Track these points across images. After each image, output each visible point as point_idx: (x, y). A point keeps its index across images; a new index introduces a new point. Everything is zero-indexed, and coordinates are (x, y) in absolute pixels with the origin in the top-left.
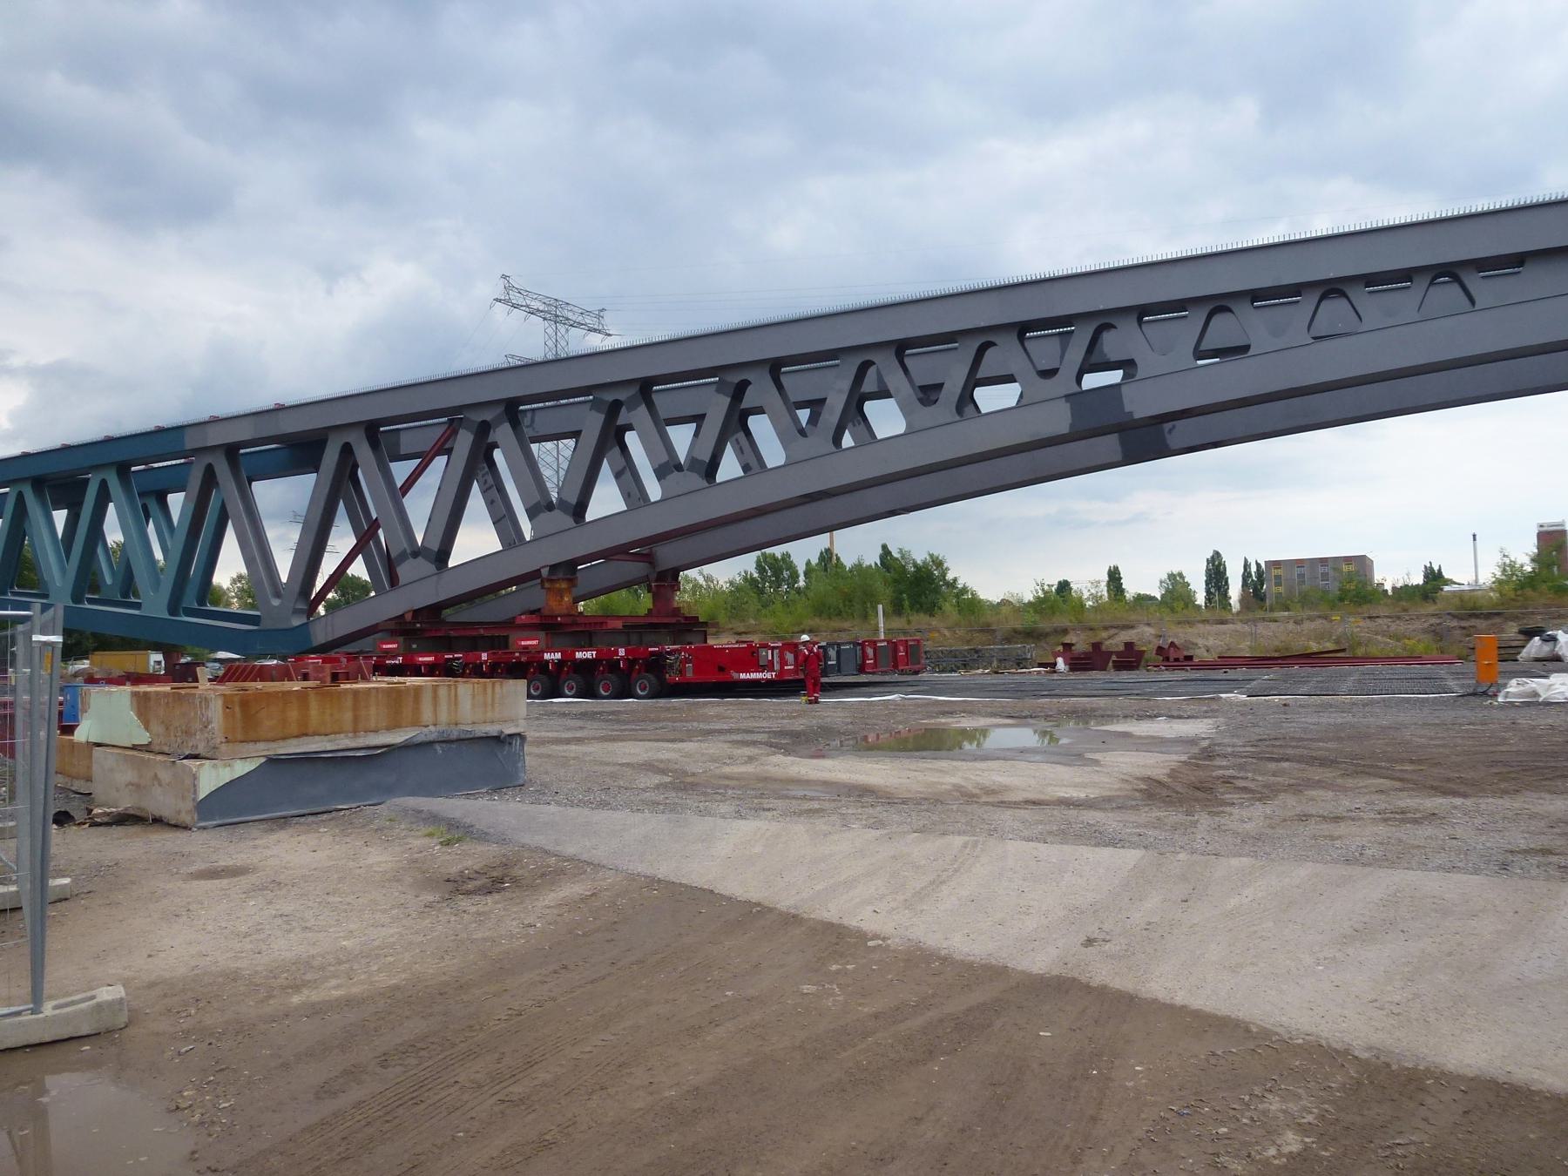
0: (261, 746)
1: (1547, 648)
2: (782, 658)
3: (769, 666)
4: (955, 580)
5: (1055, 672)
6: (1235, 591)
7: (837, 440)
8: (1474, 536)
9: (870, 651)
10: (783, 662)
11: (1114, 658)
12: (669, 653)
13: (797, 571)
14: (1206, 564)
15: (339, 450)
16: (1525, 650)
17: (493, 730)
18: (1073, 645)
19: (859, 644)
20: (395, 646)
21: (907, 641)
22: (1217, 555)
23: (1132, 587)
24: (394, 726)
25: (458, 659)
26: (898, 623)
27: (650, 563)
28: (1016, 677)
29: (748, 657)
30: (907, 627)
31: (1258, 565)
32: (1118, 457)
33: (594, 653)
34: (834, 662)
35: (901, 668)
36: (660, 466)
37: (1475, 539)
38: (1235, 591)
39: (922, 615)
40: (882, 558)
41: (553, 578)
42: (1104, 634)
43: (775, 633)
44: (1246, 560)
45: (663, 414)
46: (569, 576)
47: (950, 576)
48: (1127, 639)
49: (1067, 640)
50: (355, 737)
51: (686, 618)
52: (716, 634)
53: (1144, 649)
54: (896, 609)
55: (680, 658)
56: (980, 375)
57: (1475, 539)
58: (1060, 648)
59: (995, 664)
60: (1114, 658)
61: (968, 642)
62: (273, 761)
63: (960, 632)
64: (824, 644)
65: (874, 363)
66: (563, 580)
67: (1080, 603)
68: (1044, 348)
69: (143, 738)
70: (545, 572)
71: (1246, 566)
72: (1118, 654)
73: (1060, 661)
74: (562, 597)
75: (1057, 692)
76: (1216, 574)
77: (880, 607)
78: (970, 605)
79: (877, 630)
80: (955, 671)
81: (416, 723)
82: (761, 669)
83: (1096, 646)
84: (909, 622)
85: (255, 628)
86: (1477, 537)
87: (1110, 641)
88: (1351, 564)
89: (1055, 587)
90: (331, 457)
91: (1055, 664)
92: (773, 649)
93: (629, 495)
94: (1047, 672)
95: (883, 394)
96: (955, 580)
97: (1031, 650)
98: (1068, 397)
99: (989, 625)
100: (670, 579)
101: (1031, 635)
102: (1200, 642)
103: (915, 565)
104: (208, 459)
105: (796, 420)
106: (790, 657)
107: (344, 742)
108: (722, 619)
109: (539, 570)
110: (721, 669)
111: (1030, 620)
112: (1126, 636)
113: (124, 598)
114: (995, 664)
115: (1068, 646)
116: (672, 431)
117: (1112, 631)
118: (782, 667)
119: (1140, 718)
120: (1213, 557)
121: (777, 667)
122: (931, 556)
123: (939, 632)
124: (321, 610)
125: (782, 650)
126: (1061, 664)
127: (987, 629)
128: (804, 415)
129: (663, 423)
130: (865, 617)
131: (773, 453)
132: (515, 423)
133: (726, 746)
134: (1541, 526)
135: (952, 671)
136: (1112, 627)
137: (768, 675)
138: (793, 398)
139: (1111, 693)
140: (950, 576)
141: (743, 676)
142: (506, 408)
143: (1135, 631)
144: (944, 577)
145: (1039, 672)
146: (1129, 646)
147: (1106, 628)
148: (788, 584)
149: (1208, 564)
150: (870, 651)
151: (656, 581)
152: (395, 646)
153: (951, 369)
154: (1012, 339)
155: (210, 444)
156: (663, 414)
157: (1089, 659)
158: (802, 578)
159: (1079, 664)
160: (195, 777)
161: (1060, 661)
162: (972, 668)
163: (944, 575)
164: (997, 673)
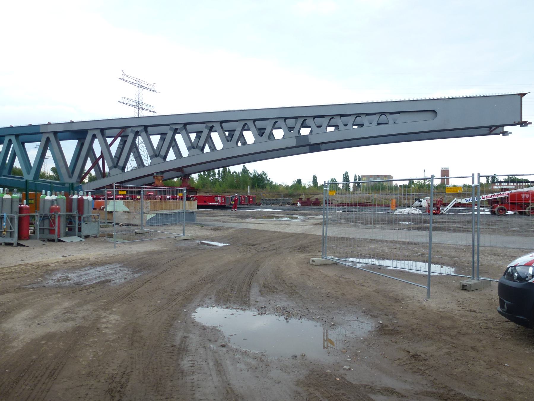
0: (156, 211)
1: (419, 203)
2: (221, 199)
3: (218, 201)
4: (269, 179)
5: (297, 206)
6: (351, 186)
7: (237, 143)
8: (424, 170)
9: (243, 199)
10: (222, 200)
11: (313, 202)
12: (191, 197)
13: (215, 173)
14: (343, 175)
15: (92, 136)
16: (414, 204)
17: (191, 210)
18: (302, 199)
19: (240, 197)
20: (110, 193)
21: (252, 196)
22: (347, 173)
23: (320, 183)
24: (176, 209)
25: (130, 197)
26: (254, 191)
27: (182, 172)
28: (287, 207)
29: (213, 199)
30: (256, 192)
31: (359, 177)
32: (309, 151)
33: (170, 197)
34: (223, 202)
35: (250, 203)
36: (189, 147)
37: (424, 171)
38: (351, 186)
39: (260, 189)
40: (243, 169)
41: (157, 176)
42: (311, 196)
43: (217, 193)
44: (355, 175)
45: (107, 135)
46: (162, 176)
47: (268, 178)
48: (317, 198)
49: (301, 197)
50: (170, 210)
51: (191, 188)
52: (199, 192)
53: (321, 200)
54: (253, 187)
55: (194, 198)
56: (275, 127)
57: (424, 171)
58: (299, 199)
59: (281, 203)
60: (313, 202)
61: (273, 197)
62: (158, 214)
63: (271, 194)
64: (231, 196)
65: (247, 124)
66: (160, 176)
67: (305, 187)
68: (291, 122)
69: (128, 210)
70: (155, 174)
71: (355, 177)
72: (314, 202)
73: (299, 203)
74: (159, 181)
75: (298, 210)
76: (346, 178)
77: (249, 186)
78: (274, 188)
79: (247, 192)
80: (270, 205)
81: (179, 209)
82: (216, 202)
83: (308, 199)
84: (257, 191)
85: (63, 186)
86: (425, 171)
87: (312, 198)
88: (372, 178)
89: (297, 181)
90: (44, 139)
91: (297, 204)
92: (219, 197)
93: (176, 153)
94: (295, 206)
95: (249, 130)
96: (269, 179)
97: (290, 200)
98: (295, 137)
99: (279, 192)
100: (187, 177)
101: (291, 195)
102: (336, 199)
103: (258, 174)
104: (47, 135)
105: (225, 134)
106: (223, 199)
107: (168, 211)
108: (200, 188)
109: (153, 174)
110: (205, 202)
111: (289, 191)
112: (316, 197)
113: (9, 175)
114: (281, 203)
115: (301, 199)
116: (191, 135)
117: (313, 195)
118: (221, 202)
119: (317, 215)
120: (345, 174)
121: (220, 201)
122: (263, 172)
123: (265, 194)
124: (86, 180)
125: (221, 197)
126: (299, 203)
127: (279, 194)
128: (227, 133)
129: (188, 133)
130: (244, 189)
131: (219, 145)
132: (146, 132)
133: (228, 218)
134: (442, 168)
135: (269, 205)
136: (313, 194)
137: (218, 204)
138: (225, 129)
139: (311, 210)
140: (268, 178)
141: (211, 204)
142: (144, 127)
143: (319, 196)
144: (266, 178)
145: (293, 206)
146: (317, 199)
147: (311, 195)
148: (212, 177)
149: (344, 176)
150: (243, 199)
151: (184, 177)
152: (110, 193)
153: (268, 125)
154: (283, 120)
155: (49, 131)
156: (189, 131)
157: (306, 202)
158: (217, 175)
159: (304, 204)
160: (146, 217)
161: (299, 203)
162: (275, 204)
163: (266, 177)
164: (282, 206)
